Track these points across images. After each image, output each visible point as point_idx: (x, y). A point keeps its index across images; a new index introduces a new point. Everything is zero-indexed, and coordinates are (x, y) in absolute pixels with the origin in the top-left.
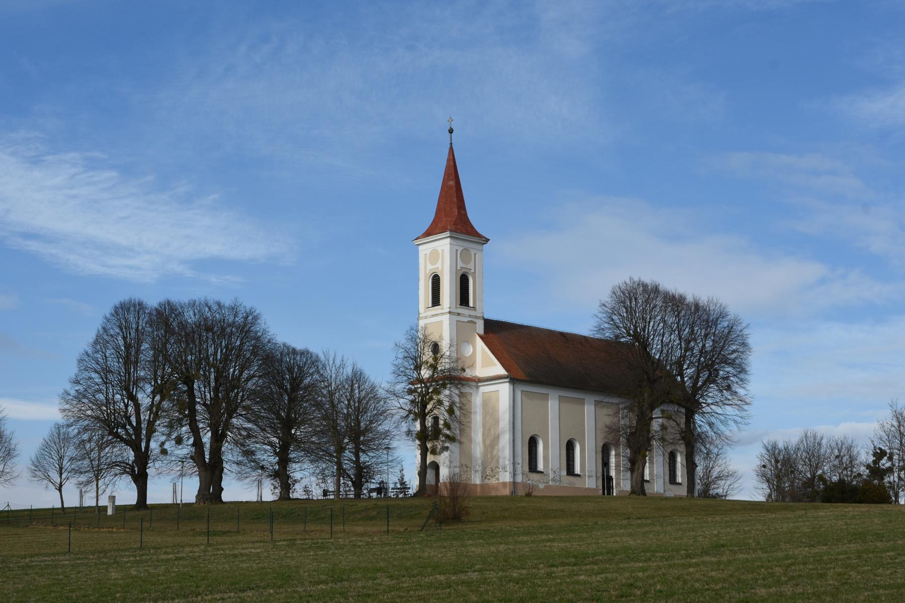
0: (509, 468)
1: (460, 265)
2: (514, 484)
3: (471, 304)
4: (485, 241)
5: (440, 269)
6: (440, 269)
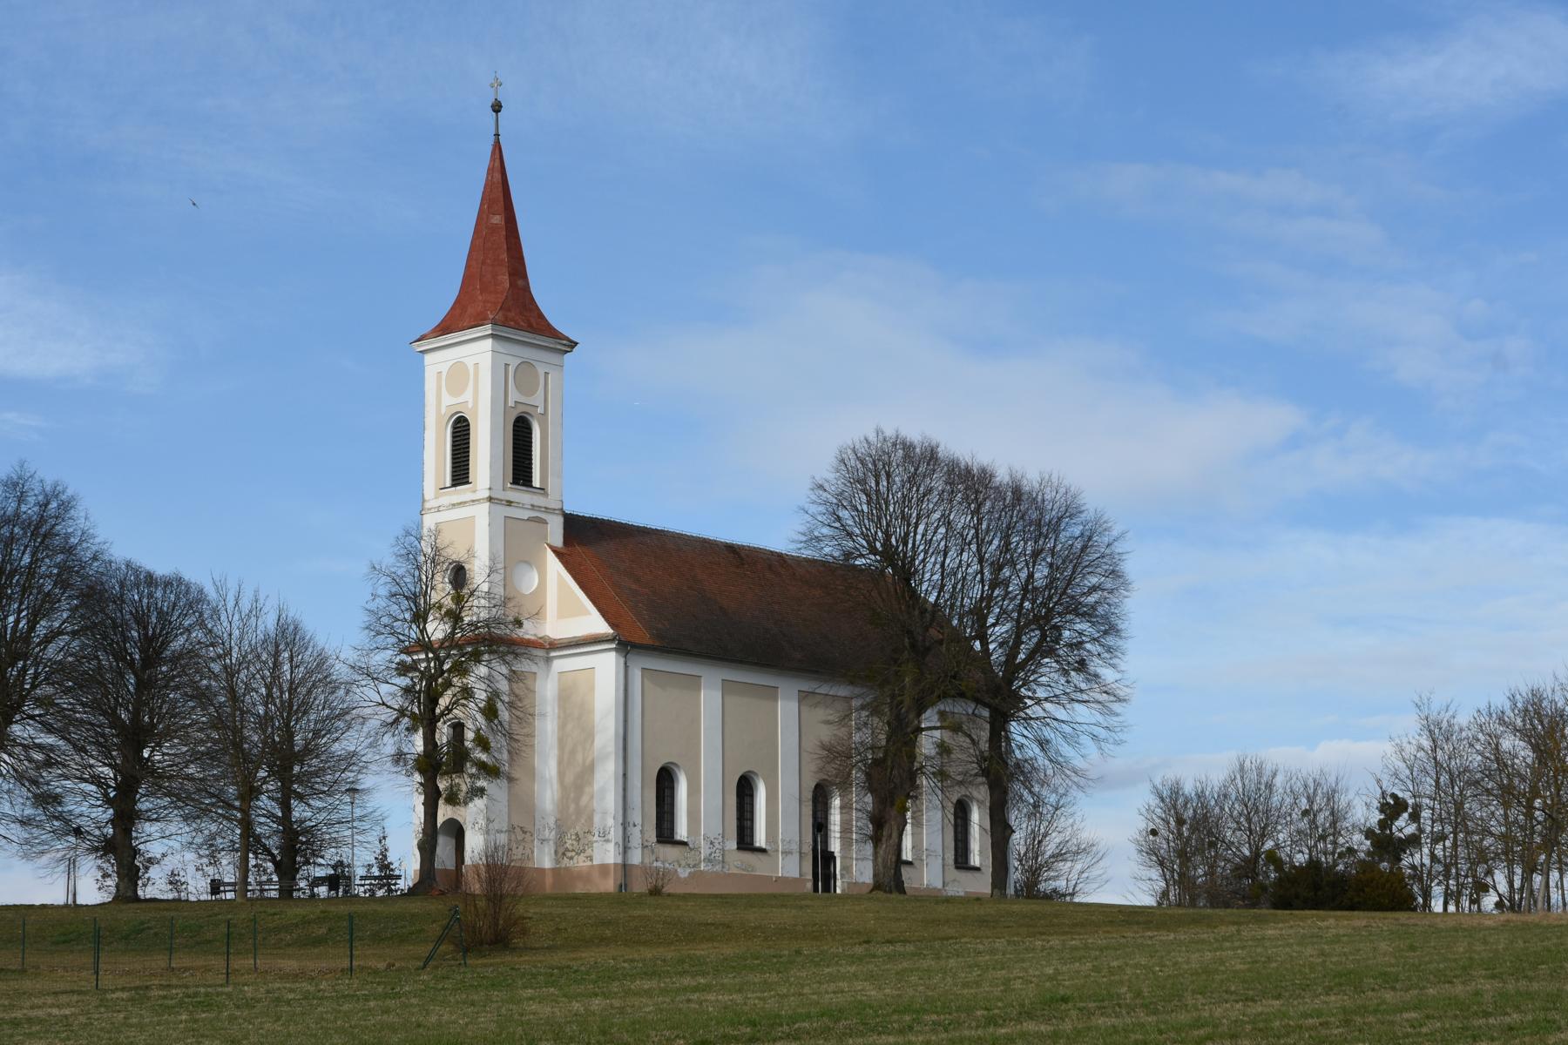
0: (615, 834)
2: (625, 868)
3: (536, 482)
5: (470, 406)
6: (470, 406)
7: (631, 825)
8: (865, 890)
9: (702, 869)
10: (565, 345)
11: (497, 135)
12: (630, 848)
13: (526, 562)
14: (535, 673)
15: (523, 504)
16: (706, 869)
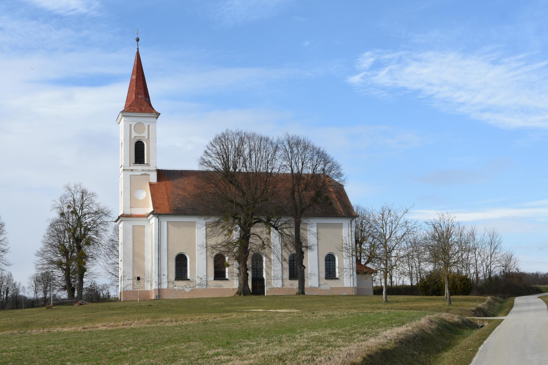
0: (155, 278)
1: (134, 134)
2: (159, 290)
3: (146, 163)
4: (158, 115)
7: (162, 275)
8: (233, 294)
9: (197, 288)
10: (154, 115)
11: (138, 49)
12: (162, 283)
13: (142, 189)
14: (343, 223)
15: (138, 170)
16: (199, 288)
